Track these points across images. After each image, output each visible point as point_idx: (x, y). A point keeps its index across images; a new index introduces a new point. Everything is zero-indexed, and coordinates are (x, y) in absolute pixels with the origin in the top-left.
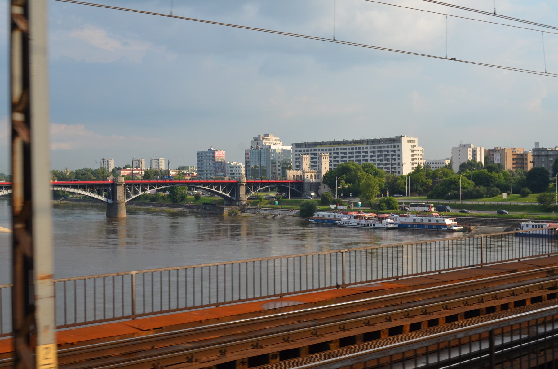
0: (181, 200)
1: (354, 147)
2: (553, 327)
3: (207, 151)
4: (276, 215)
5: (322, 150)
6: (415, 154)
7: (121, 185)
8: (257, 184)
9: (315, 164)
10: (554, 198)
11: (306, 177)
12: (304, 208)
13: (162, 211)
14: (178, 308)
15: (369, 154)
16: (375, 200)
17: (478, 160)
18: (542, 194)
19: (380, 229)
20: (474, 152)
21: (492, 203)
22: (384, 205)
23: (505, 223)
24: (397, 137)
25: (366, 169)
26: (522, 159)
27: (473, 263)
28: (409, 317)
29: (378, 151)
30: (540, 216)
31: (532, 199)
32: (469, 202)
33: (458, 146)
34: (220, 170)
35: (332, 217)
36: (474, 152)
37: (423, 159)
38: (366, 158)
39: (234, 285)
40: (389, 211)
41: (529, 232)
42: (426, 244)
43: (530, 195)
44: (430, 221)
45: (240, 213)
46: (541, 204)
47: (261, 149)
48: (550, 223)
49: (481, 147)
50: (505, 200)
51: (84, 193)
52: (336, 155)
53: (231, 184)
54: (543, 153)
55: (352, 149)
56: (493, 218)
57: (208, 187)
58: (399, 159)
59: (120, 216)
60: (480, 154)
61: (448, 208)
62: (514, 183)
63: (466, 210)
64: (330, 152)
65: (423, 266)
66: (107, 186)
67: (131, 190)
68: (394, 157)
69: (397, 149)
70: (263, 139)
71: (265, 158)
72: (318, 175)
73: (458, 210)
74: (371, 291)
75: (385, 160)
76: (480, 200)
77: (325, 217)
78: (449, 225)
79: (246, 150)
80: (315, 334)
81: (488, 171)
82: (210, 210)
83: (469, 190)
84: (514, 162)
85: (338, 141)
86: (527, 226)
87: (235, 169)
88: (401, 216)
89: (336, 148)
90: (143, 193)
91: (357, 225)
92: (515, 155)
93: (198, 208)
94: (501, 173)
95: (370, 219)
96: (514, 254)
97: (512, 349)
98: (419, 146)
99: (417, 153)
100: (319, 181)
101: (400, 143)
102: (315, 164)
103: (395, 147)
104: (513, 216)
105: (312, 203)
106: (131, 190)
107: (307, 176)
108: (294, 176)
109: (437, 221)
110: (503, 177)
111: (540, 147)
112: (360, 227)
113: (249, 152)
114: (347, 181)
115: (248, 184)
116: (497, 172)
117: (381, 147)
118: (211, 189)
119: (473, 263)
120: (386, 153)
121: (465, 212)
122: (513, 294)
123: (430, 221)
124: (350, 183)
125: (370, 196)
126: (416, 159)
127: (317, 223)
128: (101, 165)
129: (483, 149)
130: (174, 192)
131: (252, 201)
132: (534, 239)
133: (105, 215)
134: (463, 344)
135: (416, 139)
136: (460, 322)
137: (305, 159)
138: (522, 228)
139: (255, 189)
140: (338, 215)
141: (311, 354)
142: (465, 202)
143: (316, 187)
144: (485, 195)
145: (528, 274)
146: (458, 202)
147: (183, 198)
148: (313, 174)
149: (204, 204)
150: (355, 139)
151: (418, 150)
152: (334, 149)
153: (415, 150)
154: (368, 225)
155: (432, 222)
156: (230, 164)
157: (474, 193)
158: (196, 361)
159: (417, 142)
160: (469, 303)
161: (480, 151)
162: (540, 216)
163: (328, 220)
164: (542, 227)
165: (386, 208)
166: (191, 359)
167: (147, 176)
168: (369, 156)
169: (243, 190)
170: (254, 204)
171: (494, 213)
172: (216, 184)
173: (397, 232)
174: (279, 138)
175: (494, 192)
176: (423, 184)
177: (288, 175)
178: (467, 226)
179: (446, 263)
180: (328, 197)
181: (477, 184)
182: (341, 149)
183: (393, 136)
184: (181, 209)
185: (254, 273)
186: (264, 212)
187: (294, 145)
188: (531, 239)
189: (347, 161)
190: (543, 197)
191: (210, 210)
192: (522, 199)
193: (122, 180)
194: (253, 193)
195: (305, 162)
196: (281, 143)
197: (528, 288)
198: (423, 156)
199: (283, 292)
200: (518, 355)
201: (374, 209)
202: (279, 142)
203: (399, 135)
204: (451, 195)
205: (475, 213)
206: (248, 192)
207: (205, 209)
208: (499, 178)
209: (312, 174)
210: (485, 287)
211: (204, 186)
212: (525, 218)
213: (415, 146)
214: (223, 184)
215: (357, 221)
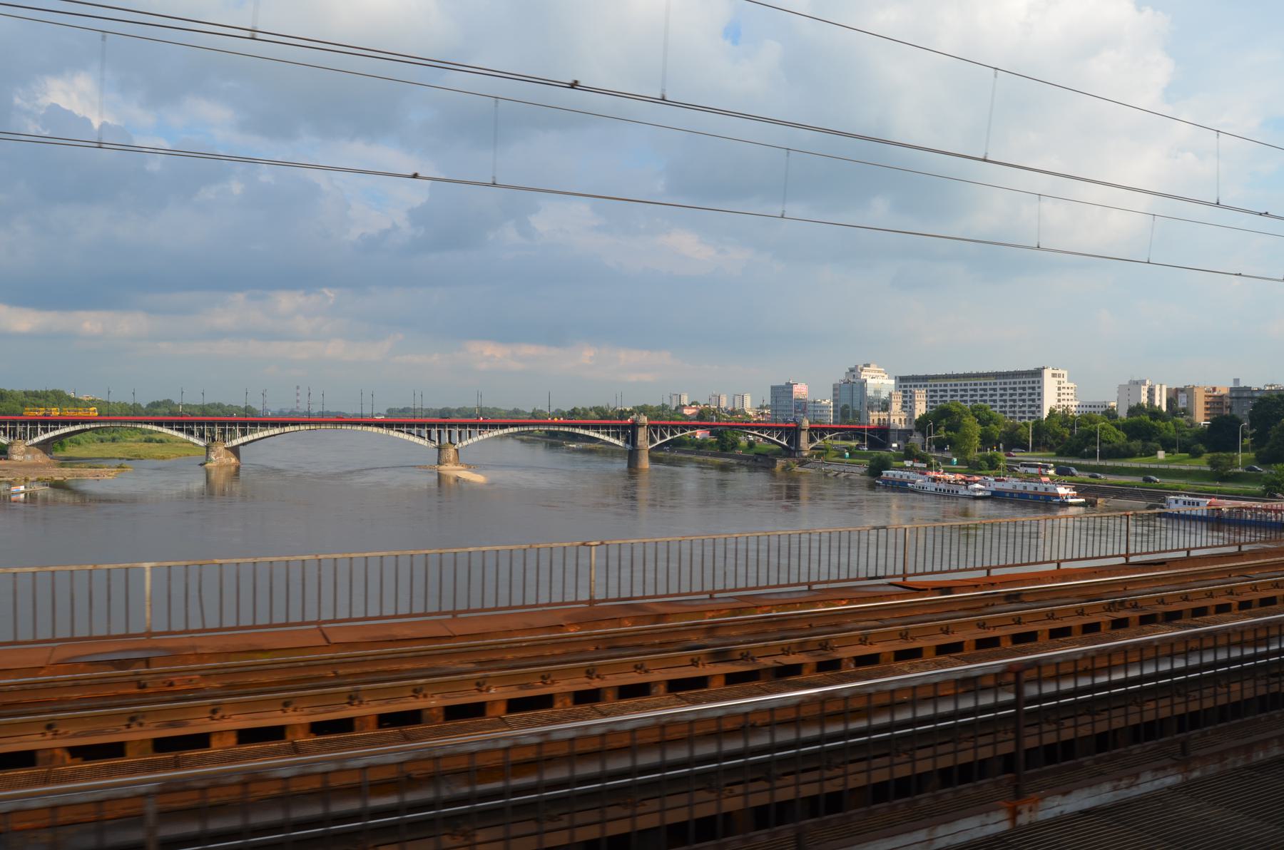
0: (732, 448)
1: (978, 382)
2: (996, 697)
3: (784, 384)
4: (840, 473)
5: (915, 386)
6: (1064, 394)
7: (643, 426)
8: (676, 427)
9: (908, 405)
10: (1235, 461)
11: (892, 421)
12: (874, 464)
13: (690, 460)
14: (483, 607)
15: (999, 392)
16: (974, 455)
17: (1157, 404)
18: (1216, 454)
19: (965, 497)
20: (1151, 392)
21: (1143, 465)
22: (985, 463)
23: (1150, 495)
24: (1038, 369)
25: (977, 413)
26: (1221, 402)
27: (679, 588)
28: (1054, 619)
29: (1011, 389)
30: (1206, 487)
31: (1201, 464)
32: (1110, 463)
33: (1127, 383)
34: (800, 410)
35: (905, 478)
36: (1151, 392)
37: (1076, 400)
38: (994, 398)
39: (540, 578)
40: (990, 472)
41: (1179, 512)
42: (1000, 524)
43: (1205, 454)
44: (1036, 488)
45: (797, 469)
46: (1214, 468)
47: (854, 383)
48: (1213, 500)
49: (1161, 385)
50: (1162, 462)
51: (170, 432)
52: (953, 393)
53: (789, 429)
54: (1245, 395)
55: (976, 384)
56: (1134, 487)
57: (759, 432)
58: (1039, 399)
59: (640, 467)
60: (1161, 395)
61: (1074, 471)
62: (1189, 438)
63: (1098, 475)
64: (905, 389)
65: (866, 564)
66: (625, 427)
67: (656, 434)
68: (1033, 397)
69: (1036, 385)
70: (862, 370)
72: (910, 419)
73: (1087, 474)
74: (926, 590)
75: (990, 401)
76: (1129, 460)
77: (896, 477)
78: (1062, 495)
79: (834, 385)
80: (904, 636)
81: (1151, 419)
82: (761, 462)
83: (1115, 445)
84: (1208, 406)
85: (957, 374)
86: (1177, 502)
87: (821, 409)
88: (996, 480)
89: (953, 383)
90: (672, 437)
91: (934, 490)
92: (1210, 396)
93: (748, 459)
94: (1170, 422)
95: (956, 482)
96: (1199, 540)
97: (1256, 664)
98: (1068, 382)
99: (1066, 391)
100: (911, 428)
101: (1041, 376)
102: (908, 405)
103: (1034, 382)
104: (1166, 486)
105: (886, 457)
106: (656, 434)
108: (879, 419)
109: (1046, 489)
110: (1172, 428)
111: (1242, 385)
112: (939, 494)
113: (838, 387)
114: (948, 428)
115: (811, 429)
116: (1163, 421)
117: (1015, 383)
119: (679, 588)
120: (1021, 391)
121: (1096, 477)
122: (1051, 616)
123: (1036, 488)
124: (951, 431)
125: (966, 450)
126: (1064, 400)
127: (886, 486)
128: (734, 403)
129: (1164, 388)
130: (722, 437)
131: (817, 451)
132: (1188, 523)
133: (626, 465)
134: (897, 704)
135: (1065, 373)
136: (1132, 630)
138: (1169, 505)
139: (822, 436)
140: (912, 475)
141: (941, 654)
142: (1102, 463)
143: (904, 435)
144: (1138, 454)
145: (88, 681)
146: (1093, 463)
147: (735, 445)
148: (903, 419)
149: (756, 454)
150: (980, 371)
151: (1068, 388)
152: (951, 385)
153: (1064, 388)
154: (948, 491)
155: (1039, 490)
156: (821, 402)
157: (1122, 450)
158: (598, 677)
159: (1066, 376)
160: (1086, 612)
161: (1161, 390)
162: (1206, 487)
163: (900, 482)
164: (1198, 504)
165: (986, 467)
166: (865, 641)
167: (701, 415)
168: (949, 396)
169: (804, 437)
170: (819, 456)
171: (1138, 480)
172: (769, 428)
173: (988, 504)
174: (883, 370)
175: (1151, 450)
176: (1055, 435)
177: (871, 418)
178: (1092, 498)
179: (1083, 548)
180: (913, 450)
181: (1130, 438)
182: (981, 384)
183: (1032, 368)
184: (728, 460)
186: (827, 468)
187: (898, 379)
188: (1182, 523)
189: (948, 401)
190: (1217, 459)
191: (761, 462)
192: (1191, 460)
194: (819, 441)
195: (895, 402)
196: (886, 376)
197: (1211, 591)
198: (1075, 396)
199: (459, 608)
200: (1105, 707)
201: (971, 468)
202: (883, 374)
203: (1041, 366)
204: (1088, 451)
205: (1112, 479)
206: (812, 440)
207: (756, 460)
208: (1166, 429)
210: (810, 625)
211: (752, 430)
212: (1182, 490)
213: (1064, 382)
214: (778, 428)
215: (935, 485)
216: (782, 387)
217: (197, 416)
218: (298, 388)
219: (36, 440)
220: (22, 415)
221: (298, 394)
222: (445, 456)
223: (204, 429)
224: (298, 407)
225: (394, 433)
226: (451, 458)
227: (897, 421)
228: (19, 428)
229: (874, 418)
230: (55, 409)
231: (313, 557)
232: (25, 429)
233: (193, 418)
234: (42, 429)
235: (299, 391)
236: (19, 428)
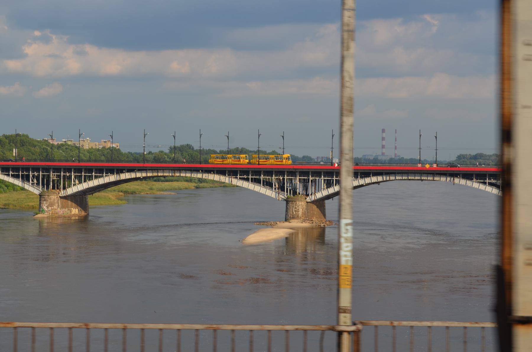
51: (482, 187)
195: (451, 179)
217: (102, 161)
218: (383, 131)
219: (70, 191)
220: (206, 162)
221: (395, 143)
222: (292, 211)
223: (284, 179)
224: (396, 154)
225: (475, 185)
226: (300, 213)
228: (53, 176)
230: (244, 156)
231: (388, 323)
232: (59, 176)
233: (82, 164)
234: (75, 177)
235: (384, 135)
236: (53, 176)
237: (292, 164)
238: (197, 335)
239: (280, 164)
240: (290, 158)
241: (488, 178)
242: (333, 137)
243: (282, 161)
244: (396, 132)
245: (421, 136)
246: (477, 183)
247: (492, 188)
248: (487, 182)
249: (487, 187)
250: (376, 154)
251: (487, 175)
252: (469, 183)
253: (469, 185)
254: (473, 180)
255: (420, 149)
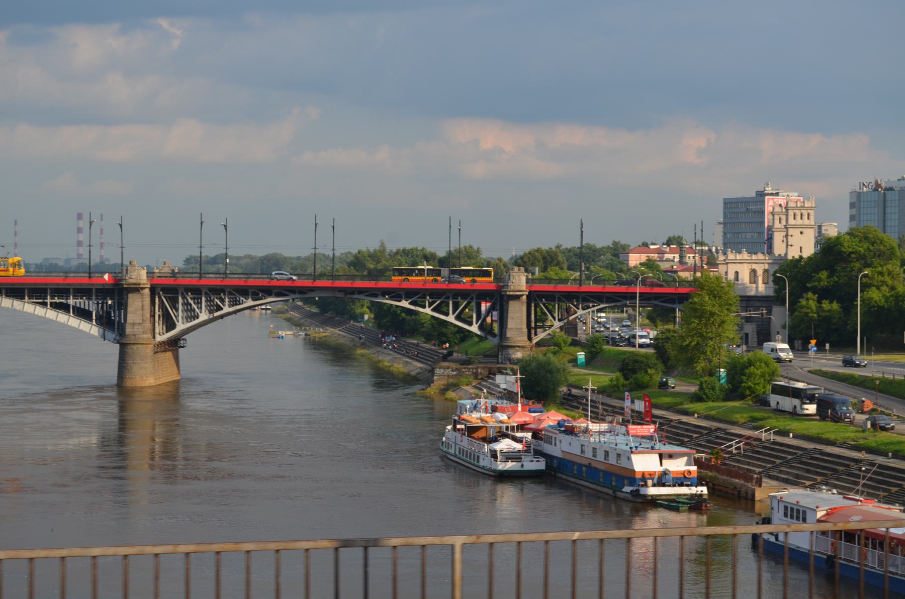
3: (754, 195)
51: (40, 311)
57: (410, 303)
71: (897, 216)
107: (737, 273)
118: (421, 310)
137: (798, 213)
148: (760, 270)
169: (517, 314)
172: (435, 294)
185: (95, 582)
193: (139, 275)
209: (754, 266)
216: (745, 201)
221: (101, 238)
225: (28, 307)
227: (745, 277)
229: (737, 267)
237: (23, 276)
238: (94, 566)
239: (4, 275)
240: (22, 263)
241: (51, 296)
242: (91, 225)
243: (7, 270)
244: (102, 219)
245: (318, 226)
246: (31, 305)
247: (57, 313)
248: (49, 303)
249: (49, 310)
250: (67, 256)
251: (49, 290)
252: (17, 304)
253: (18, 308)
254: (24, 299)
255: (201, 247)
